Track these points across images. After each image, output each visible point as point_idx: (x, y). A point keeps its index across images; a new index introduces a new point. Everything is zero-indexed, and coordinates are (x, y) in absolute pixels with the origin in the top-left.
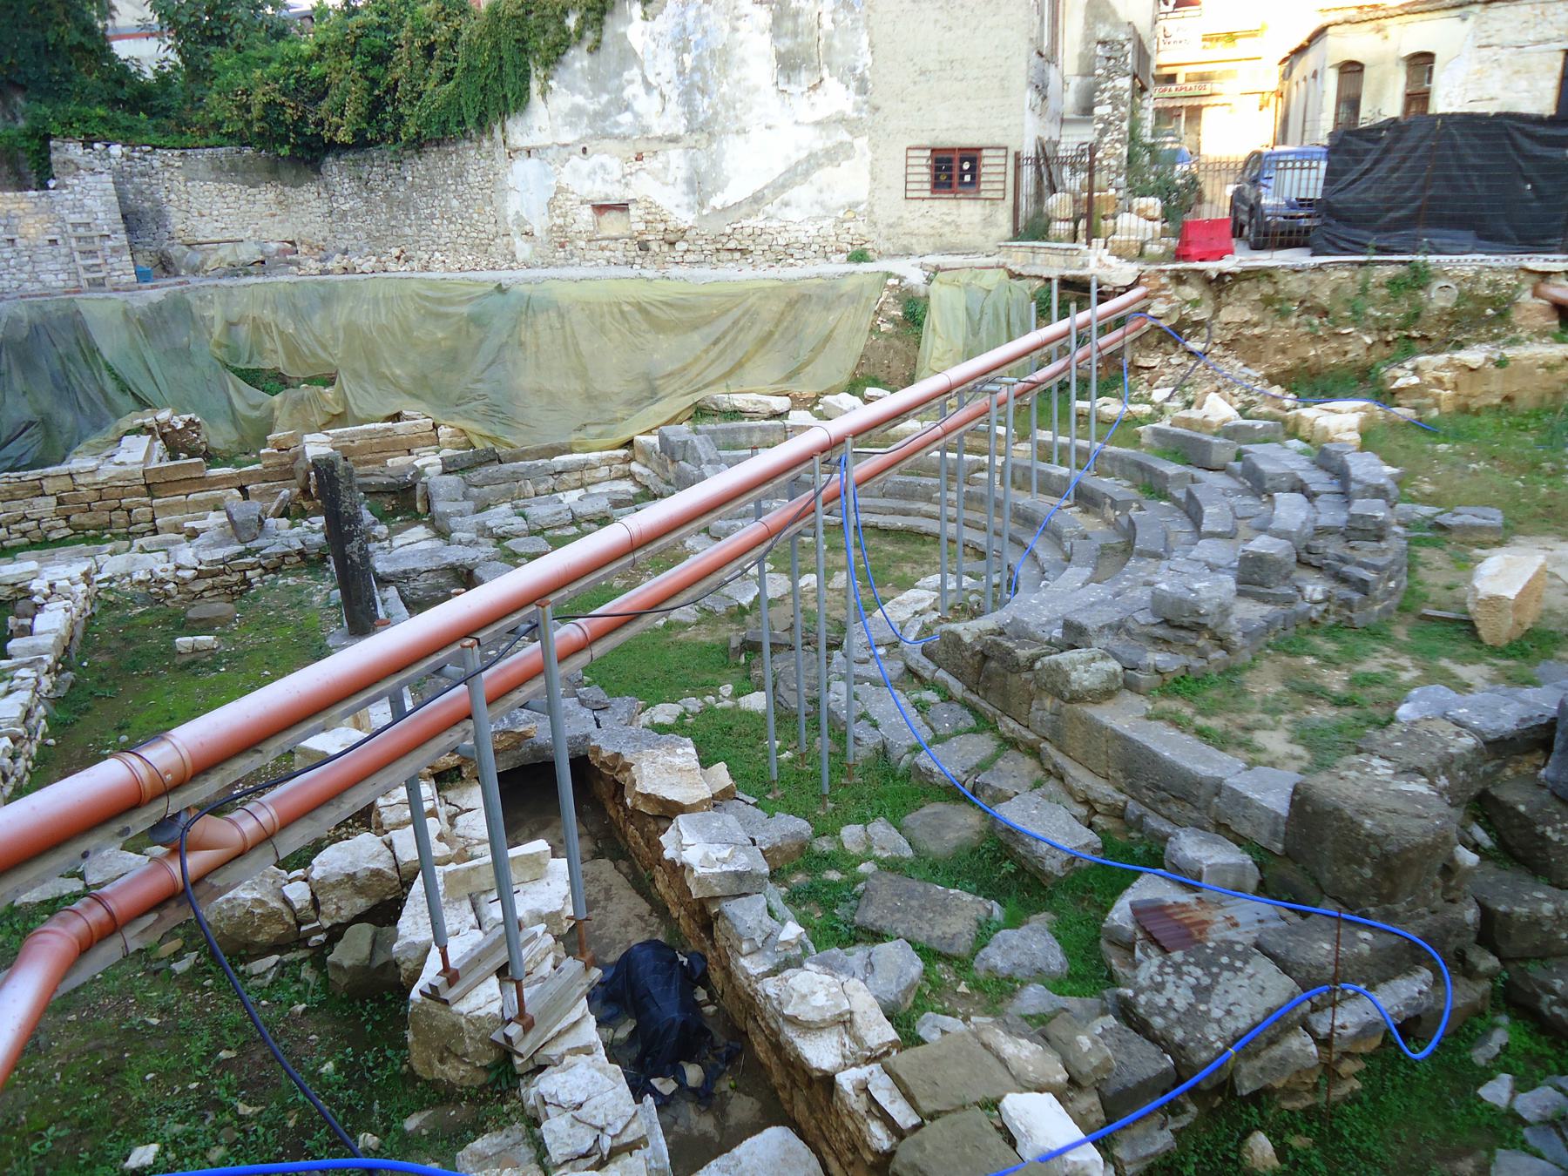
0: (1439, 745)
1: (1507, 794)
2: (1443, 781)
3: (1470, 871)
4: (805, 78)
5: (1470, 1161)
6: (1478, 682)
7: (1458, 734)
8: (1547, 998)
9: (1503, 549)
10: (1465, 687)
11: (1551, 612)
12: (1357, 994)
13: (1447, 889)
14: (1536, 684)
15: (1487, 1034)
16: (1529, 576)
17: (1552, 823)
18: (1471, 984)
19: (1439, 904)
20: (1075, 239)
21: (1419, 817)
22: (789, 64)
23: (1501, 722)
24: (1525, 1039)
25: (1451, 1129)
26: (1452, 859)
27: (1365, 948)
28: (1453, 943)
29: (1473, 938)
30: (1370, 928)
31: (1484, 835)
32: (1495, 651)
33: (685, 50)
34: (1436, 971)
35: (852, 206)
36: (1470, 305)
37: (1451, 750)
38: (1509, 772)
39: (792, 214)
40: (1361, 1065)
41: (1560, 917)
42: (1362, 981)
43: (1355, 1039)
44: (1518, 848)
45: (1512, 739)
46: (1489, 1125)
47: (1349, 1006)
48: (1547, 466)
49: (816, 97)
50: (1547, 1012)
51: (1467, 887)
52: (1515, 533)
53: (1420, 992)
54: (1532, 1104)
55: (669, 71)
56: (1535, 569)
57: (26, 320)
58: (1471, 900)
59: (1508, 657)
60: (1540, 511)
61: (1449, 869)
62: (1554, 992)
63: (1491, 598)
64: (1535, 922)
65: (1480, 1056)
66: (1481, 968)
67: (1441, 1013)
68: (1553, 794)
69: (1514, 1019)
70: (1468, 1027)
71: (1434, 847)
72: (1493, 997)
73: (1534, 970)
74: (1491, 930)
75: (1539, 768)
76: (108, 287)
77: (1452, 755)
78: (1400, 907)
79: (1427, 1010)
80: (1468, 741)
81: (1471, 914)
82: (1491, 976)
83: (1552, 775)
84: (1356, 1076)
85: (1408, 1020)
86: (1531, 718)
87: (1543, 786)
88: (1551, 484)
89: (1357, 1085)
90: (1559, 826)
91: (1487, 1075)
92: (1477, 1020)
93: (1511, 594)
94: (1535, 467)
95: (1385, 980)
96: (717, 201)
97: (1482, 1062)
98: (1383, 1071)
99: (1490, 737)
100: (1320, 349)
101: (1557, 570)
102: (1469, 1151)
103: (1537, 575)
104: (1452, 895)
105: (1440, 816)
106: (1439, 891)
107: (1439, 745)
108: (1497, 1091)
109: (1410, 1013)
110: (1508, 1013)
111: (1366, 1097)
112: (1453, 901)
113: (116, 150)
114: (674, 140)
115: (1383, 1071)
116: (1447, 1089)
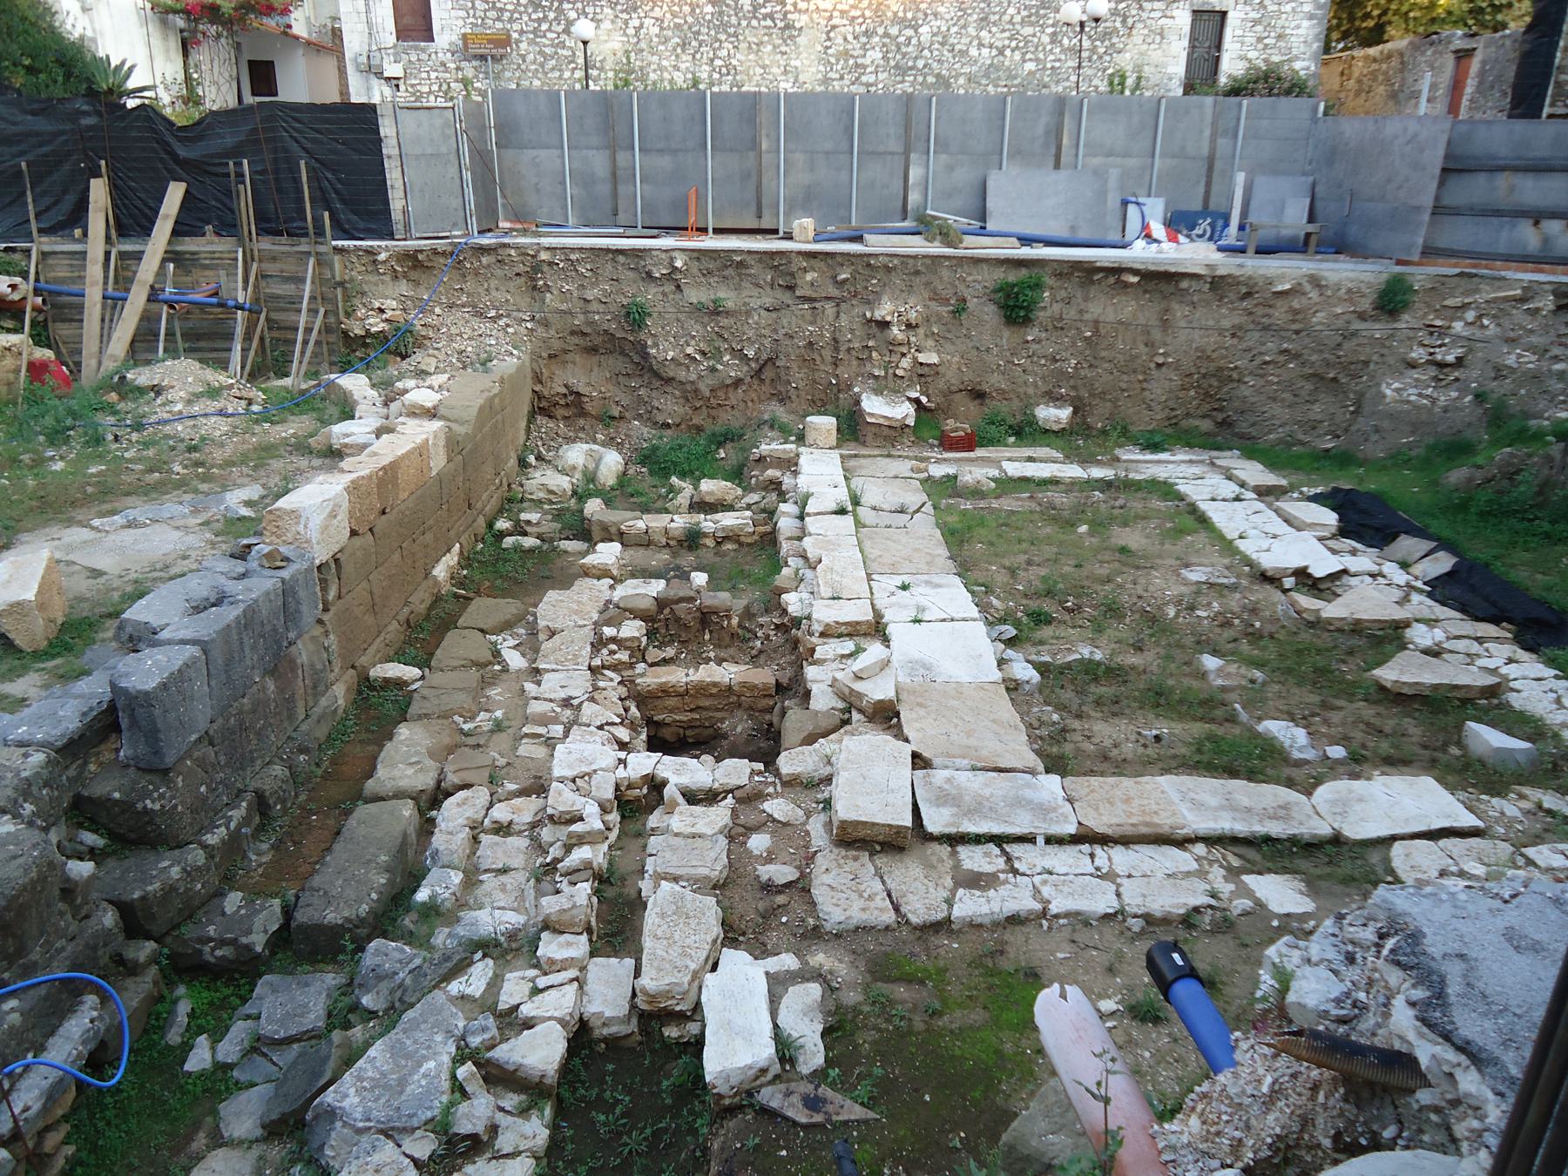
0: (9, 775)
1: (99, 789)
2: (29, 808)
3: (93, 877)
5: (202, 1135)
6: (33, 692)
7: (26, 755)
8: (207, 949)
9: (11, 552)
10: (23, 702)
11: (80, 599)
12: (27, 1068)
13: (75, 911)
14: (88, 673)
15: (172, 1012)
16: (41, 572)
17: (149, 795)
18: (138, 979)
19: (74, 927)
21: (15, 857)
23: (64, 724)
24: (205, 994)
25: (176, 1119)
26: (68, 880)
27: (15, 1018)
28: (104, 957)
29: (121, 937)
30: (12, 994)
31: (95, 837)
32: (38, 655)
34: (98, 990)
37: (24, 774)
38: (92, 767)
40: (65, 1128)
41: (189, 874)
42: (28, 1050)
43: (46, 1109)
44: (131, 833)
45: (82, 736)
46: (204, 1091)
47: (23, 1084)
48: (26, 458)
50: (212, 960)
51: (95, 895)
52: (18, 532)
53: (92, 1021)
54: (229, 1049)
56: (44, 564)
57: (581, 467)
58: (105, 904)
59: (53, 657)
60: (34, 503)
61: (69, 891)
62: (211, 940)
63: (12, 606)
64: (170, 890)
65: (174, 1037)
66: (142, 959)
67: (121, 1023)
68: (139, 769)
69: (189, 984)
70: (154, 1016)
71: (42, 879)
72: (165, 977)
73: (189, 931)
74: (134, 921)
75: (117, 750)
76: (781, 234)
77: (27, 779)
78: (35, 955)
79: (108, 1030)
80: (38, 758)
81: (109, 918)
82: (154, 960)
83: (130, 752)
84: (65, 1142)
85: (91, 1054)
86: (91, 709)
87: (127, 766)
88: (36, 475)
89: (70, 1150)
90: (156, 795)
91: (186, 1048)
92: (159, 1007)
93: (30, 595)
94: (14, 461)
95: (52, 1033)
97: (179, 1040)
98: (92, 1117)
99: (59, 744)
101: (71, 557)
102: (196, 1127)
103: (48, 569)
104: (84, 912)
105: (35, 846)
106: (69, 917)
107: (9, 775)
108: (200, 1058)
109: (92, 1046)
110: (182, 982)
111: (84, 1154)
112: (87, 917)
115: (92, 1117)
116: (157, 1087)
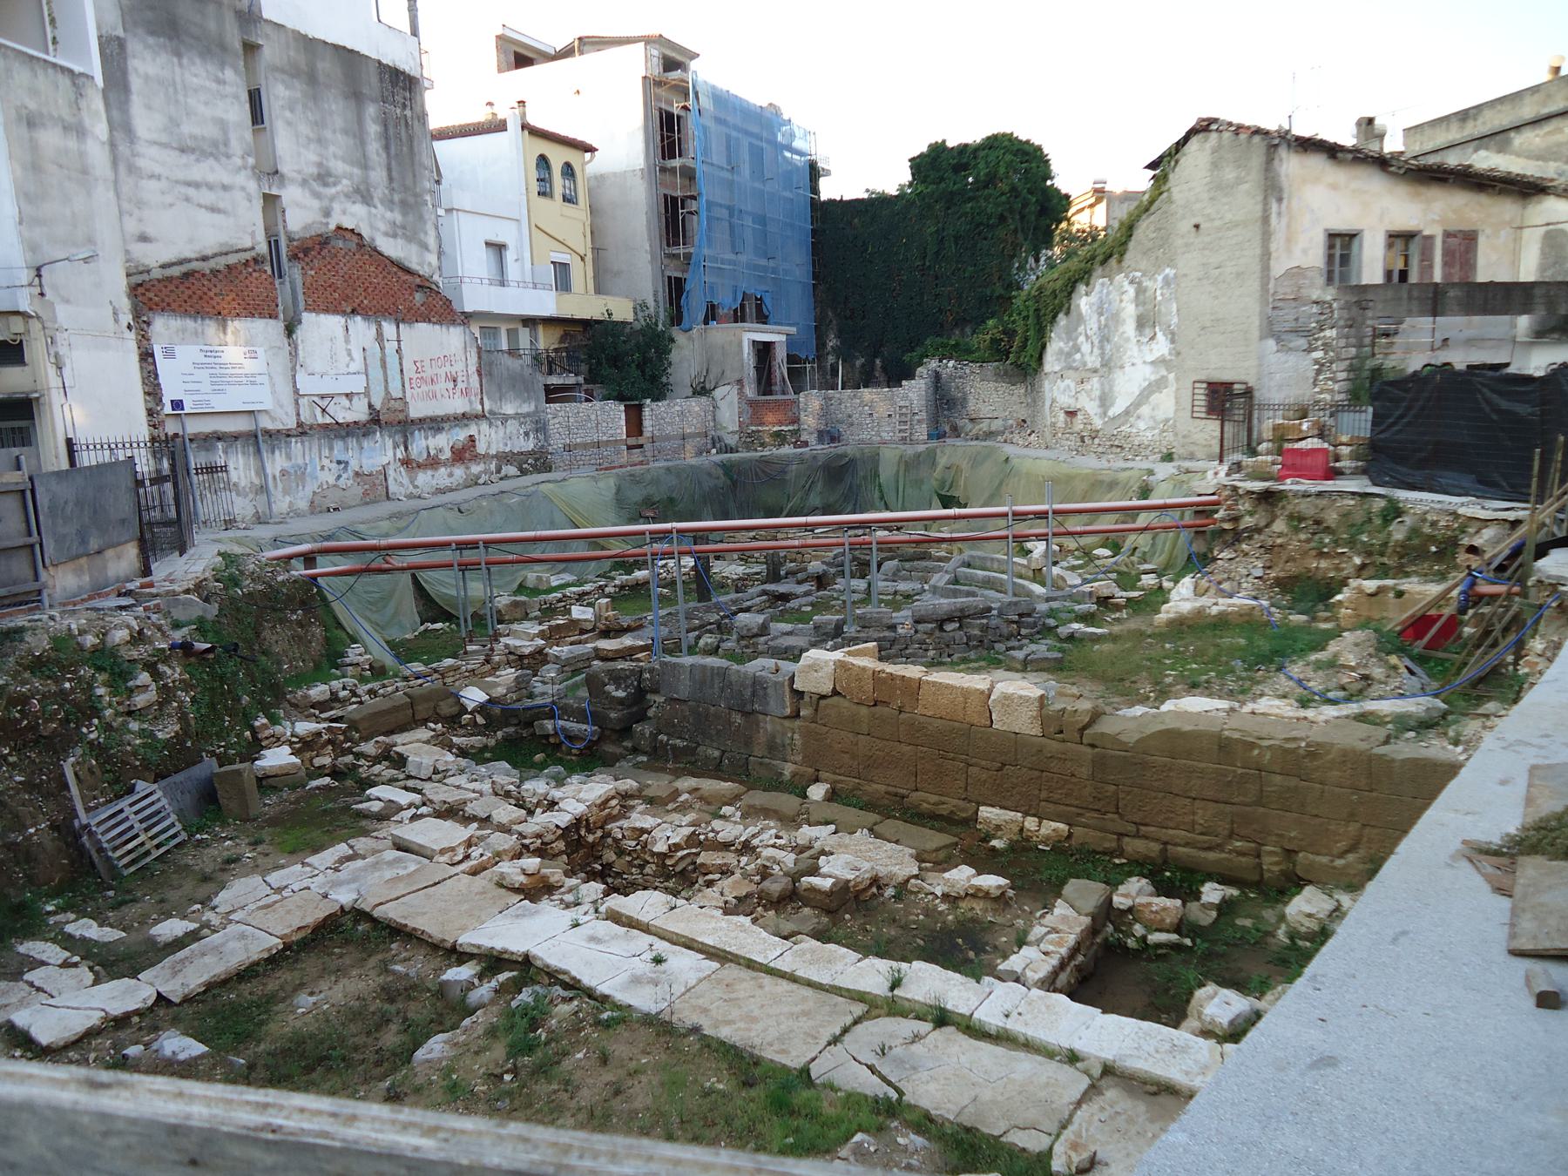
4: (1148, 332)
20: (641, 446)
22: (1142, 323)
33: (1101, 314)
35: (1167, 421)
36: (1416, 542)
39: (1142, 425)
49: (1153, 345)
55: (1095, 327)
96: (1110, 413)
100: (1324, 564)
113: (951, 363)
114: (1095, 371)
